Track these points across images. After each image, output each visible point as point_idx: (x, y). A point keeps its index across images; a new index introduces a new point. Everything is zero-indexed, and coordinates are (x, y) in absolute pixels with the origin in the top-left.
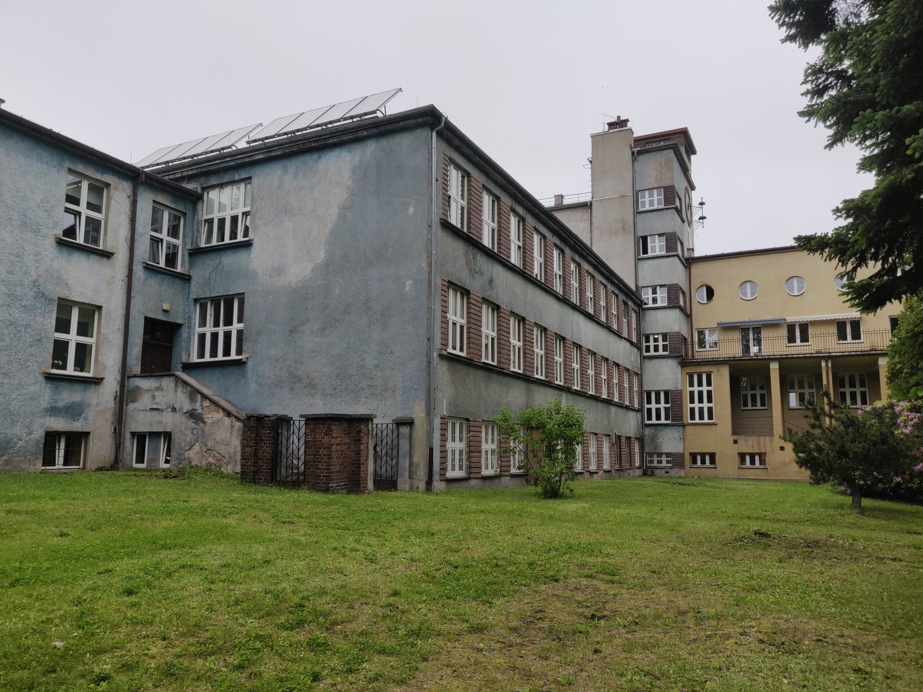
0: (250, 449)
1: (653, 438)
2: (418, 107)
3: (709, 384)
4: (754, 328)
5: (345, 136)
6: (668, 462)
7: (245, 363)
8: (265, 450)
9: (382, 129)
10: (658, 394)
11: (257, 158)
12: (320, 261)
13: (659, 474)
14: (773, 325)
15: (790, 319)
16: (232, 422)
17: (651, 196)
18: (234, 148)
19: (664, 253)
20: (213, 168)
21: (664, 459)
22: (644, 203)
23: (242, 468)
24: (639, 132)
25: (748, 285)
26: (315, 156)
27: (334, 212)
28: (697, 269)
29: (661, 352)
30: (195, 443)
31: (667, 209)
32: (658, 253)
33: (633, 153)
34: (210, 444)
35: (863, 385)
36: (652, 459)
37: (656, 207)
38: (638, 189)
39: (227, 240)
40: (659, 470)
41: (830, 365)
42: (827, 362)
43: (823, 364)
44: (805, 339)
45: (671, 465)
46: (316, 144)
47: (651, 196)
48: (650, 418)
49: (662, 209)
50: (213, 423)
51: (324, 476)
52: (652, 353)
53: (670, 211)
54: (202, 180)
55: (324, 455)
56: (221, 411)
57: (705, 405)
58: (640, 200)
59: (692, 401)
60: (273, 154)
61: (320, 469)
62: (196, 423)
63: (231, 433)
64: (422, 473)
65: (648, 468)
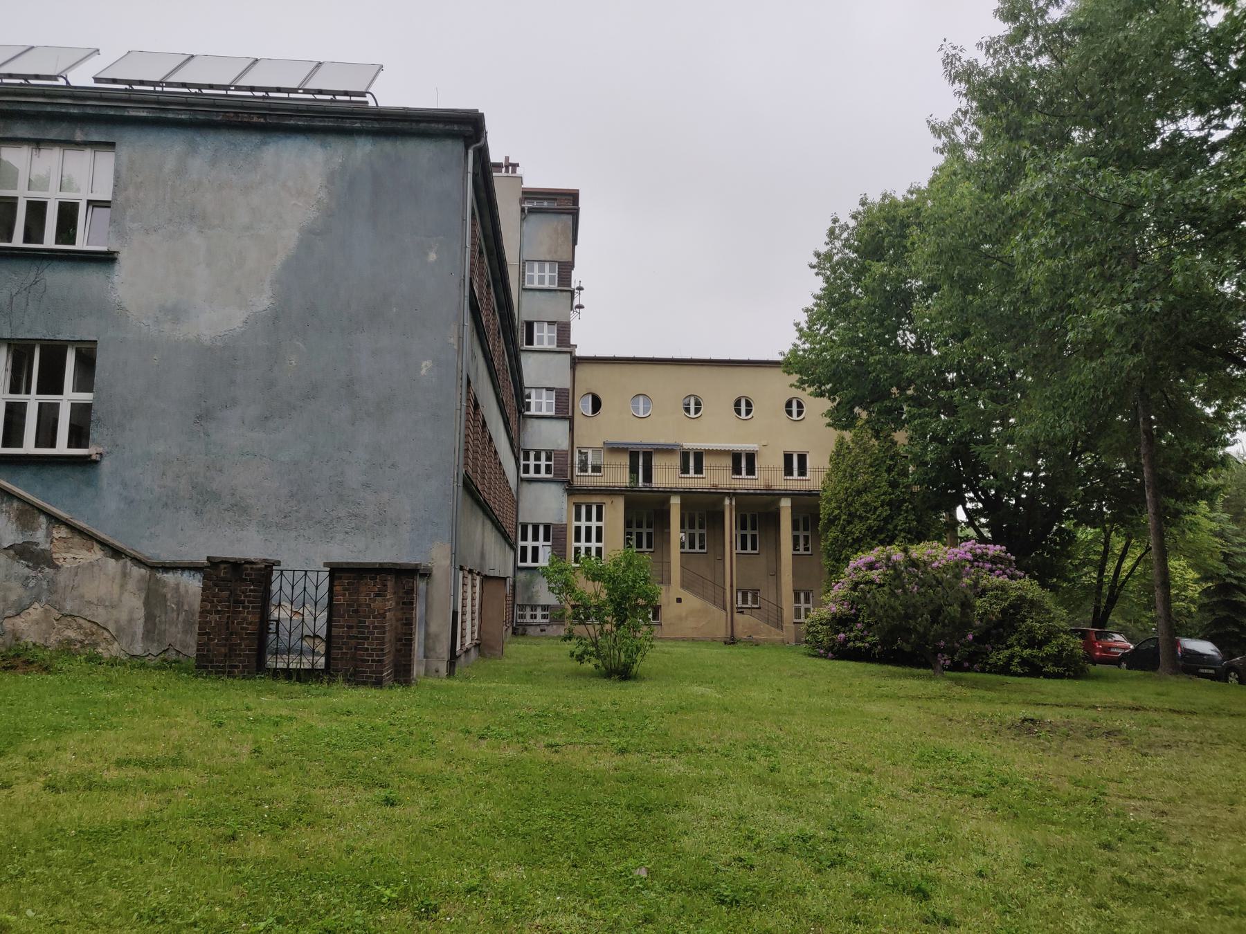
0: (217, 617)
1: (528, 586)
2: (440, 107)
3: (599, 518)
4: (644, 452)
5: (320, 121)
6: (544, 617)
7: (96, 462)
8: (244, 619)
9: (390, 125)
10: (536, 528)
11: (133, 113)
12: (261, 309)
13: (532, 633)
14: (667, 450)
15: (689, 444)
16: (125, 566)
17: (542, 270)
18: (62, 82)
19: (554, 347)
20: (24, 108)
21: (539, 612)
22: (531, 279)
23: (198, 650)
24: (530, 183)
25: (641, 398)
26: (255, 139)
27: (290, 237)
28: (583, 372)
29: (543, 474)
30: (31, 604)
31: (561, 291)
32: (546, 346)
33: (523, 210)
34: (69, 606)
35: (754, 528)
36: (534, 613)
37: (546, 285)
38: (525, 257)
39: (49, 241)
40: (533, 627)
41: (734, 503)
42: (731, 499)
43: (727, 502)
44: (699, 470)
45: (547, 621)
46: (262, 120)
47: (542, 270)
48: (524, 559)
49: (555, 290)
50: (78, 567)
51: (373, 661)
52: (532, 474)
53: (564, 293)
55: (375, 627)
56: (97, 547)
57: (594, 544)
58: (527, 273)
59: (578, 539)
60: (170, 115)
61: (367, 649)
62: (35, 568)
63: (122, 586)
64: (443, 649)
65: (519, 624)
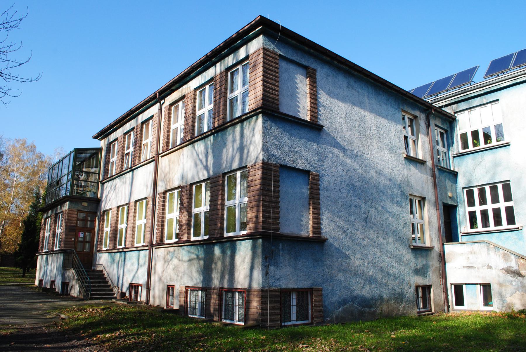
54: (454, 106)
62: (514, 277)
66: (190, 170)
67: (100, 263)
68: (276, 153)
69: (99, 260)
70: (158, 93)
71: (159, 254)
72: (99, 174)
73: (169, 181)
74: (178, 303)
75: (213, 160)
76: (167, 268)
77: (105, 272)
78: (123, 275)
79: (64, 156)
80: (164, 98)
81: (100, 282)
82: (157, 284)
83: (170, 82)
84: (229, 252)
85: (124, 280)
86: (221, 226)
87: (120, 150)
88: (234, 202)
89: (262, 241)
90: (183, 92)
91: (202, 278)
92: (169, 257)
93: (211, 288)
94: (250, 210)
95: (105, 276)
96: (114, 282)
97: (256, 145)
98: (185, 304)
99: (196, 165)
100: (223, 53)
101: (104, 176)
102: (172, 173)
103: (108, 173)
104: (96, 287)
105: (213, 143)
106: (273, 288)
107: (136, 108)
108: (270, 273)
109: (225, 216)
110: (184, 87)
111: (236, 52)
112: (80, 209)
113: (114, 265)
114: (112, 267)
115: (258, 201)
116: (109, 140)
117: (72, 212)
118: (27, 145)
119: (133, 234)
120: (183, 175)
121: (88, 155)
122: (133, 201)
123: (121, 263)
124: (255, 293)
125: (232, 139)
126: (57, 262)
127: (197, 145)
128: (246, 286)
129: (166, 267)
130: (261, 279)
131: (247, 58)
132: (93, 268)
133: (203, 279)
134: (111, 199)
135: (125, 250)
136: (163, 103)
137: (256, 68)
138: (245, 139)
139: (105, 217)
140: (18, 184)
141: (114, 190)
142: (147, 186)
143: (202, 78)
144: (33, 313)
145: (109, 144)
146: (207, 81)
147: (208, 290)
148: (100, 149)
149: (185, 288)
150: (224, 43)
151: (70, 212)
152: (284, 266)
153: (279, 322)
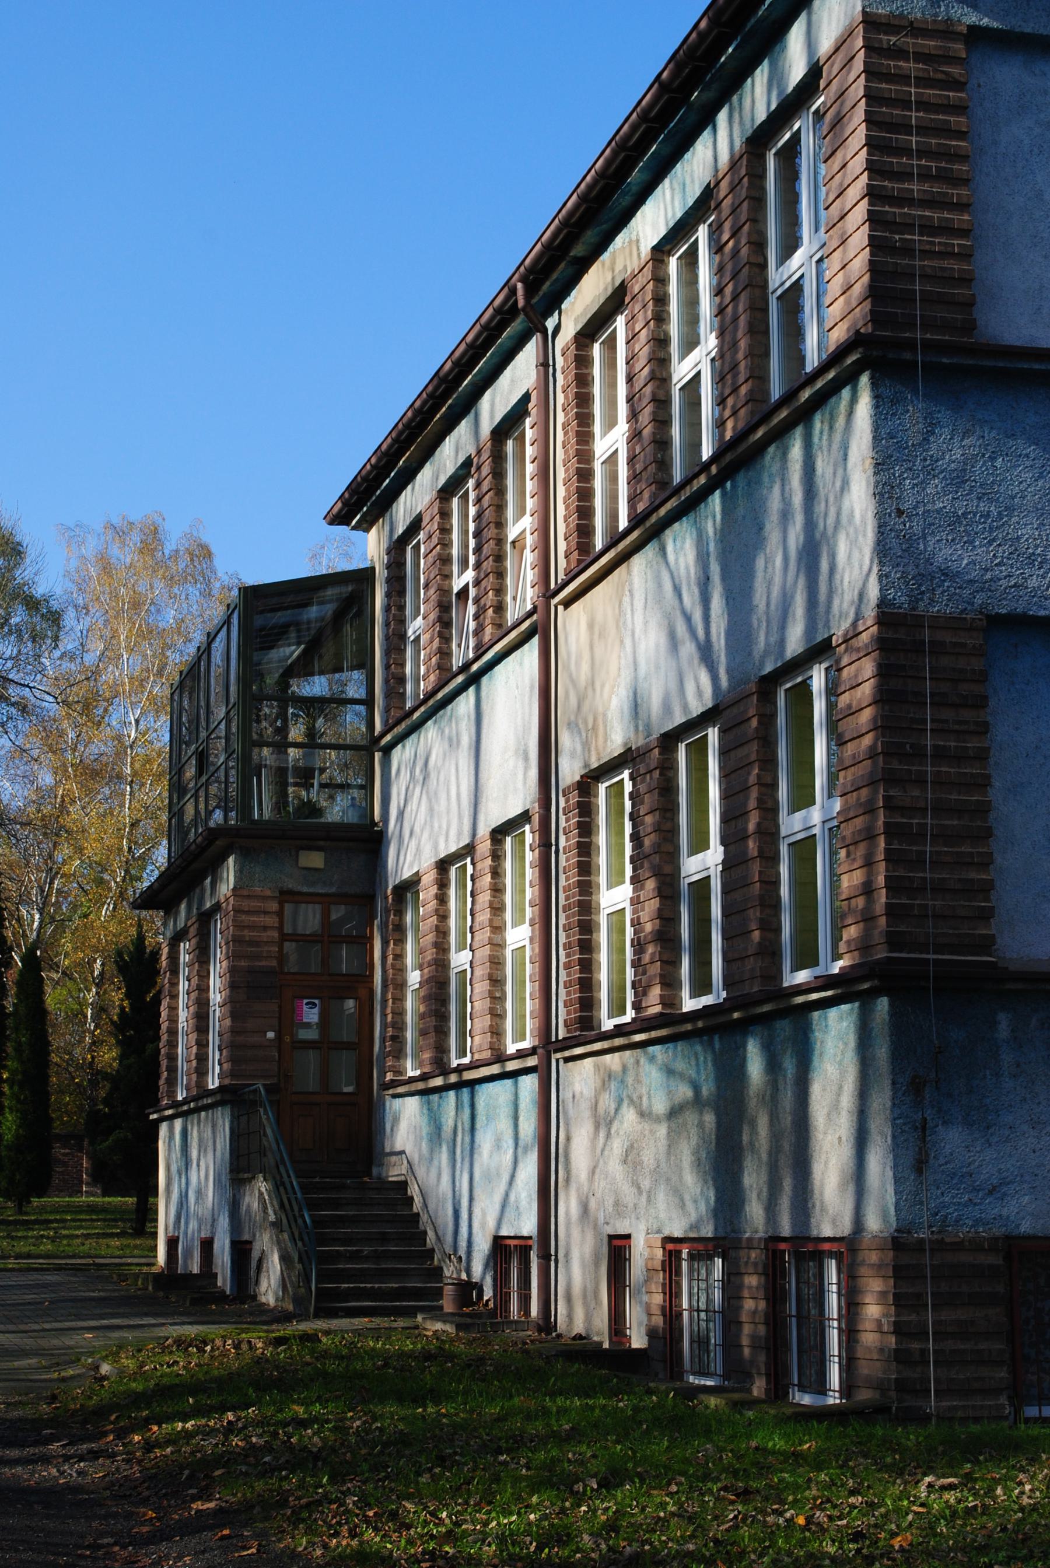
66: (657, 667)
67: (398, 1147)
68: (961, 558)
69: (392, 1130)
70: (520, 281)
71: (578, 1087)
72: (369, 702)
73: (595, 728)
74: (644, 1319)
75: (726, 616)
76: (606, 1153)
77: (414, 1190)
78: (471, 1199)
79: (210, 627)
80: (554, 302)
81: (384, 1238)
82: (576, 1233)
83: (553, 227)
84: (789, 1065)
85: (476, 1225)
86: (762, 938)
87: (432, 576)
88: (805, 819)
89: (891, 1005)
90: (619, 267)
91: (712, 1194)
92: (607, 1102)
93: (740, 1240)
94: (848, 855)
95: (415, 1210)
96: (444, 1235)
97: (856, 531)
98: (665, 1322)
99: (674, 643)
100: (723, 59)
101: (387, 710)
102: (603, 686)
103: (404, 694)
104: (366, 1259)
105: (722, 529)
106: (963, 1232)
107: (456, 364)
108: (942, 1161)
109: (785, 891)
110: (620, 240)
111: (777, 48)
112: (290, 884)
113: (440, 1152)
114: (436, 1162)
115: (870, 810)
116: (392, 531)
117: (255, 904)
118: (169, 548)
119: (493, 998)
120: (635, 694)
121: (329, 609)
122: (484, 831)
123: (463, 1139)
124: (874, 1257)
125: (781, 506)
126: (215, 1150)
127: (674, 540)
128: (845, 1228)
129: (603, 1150)
130: (890, 1189)
131: (815, 72)
132: (375, 1171)
133: (718, 1199)
134: (417, 829)
135: (469, 1075)
136: (557, 329)
137: (842, 130)
138: (819, 503)
139: (409, 918)
140: (148, 760)
141: (424, 779)
142: (526, 759)
143: (672, 189)
144: (16, 1363)
145: (398, 547)
146: (690, 208)
147: (732, 1253)
148: (366, 576)
149: (664, 1249)
150: (710, 13)
151: (246, 904)
152: (1025, 1127)
153: (1003, 1400)
